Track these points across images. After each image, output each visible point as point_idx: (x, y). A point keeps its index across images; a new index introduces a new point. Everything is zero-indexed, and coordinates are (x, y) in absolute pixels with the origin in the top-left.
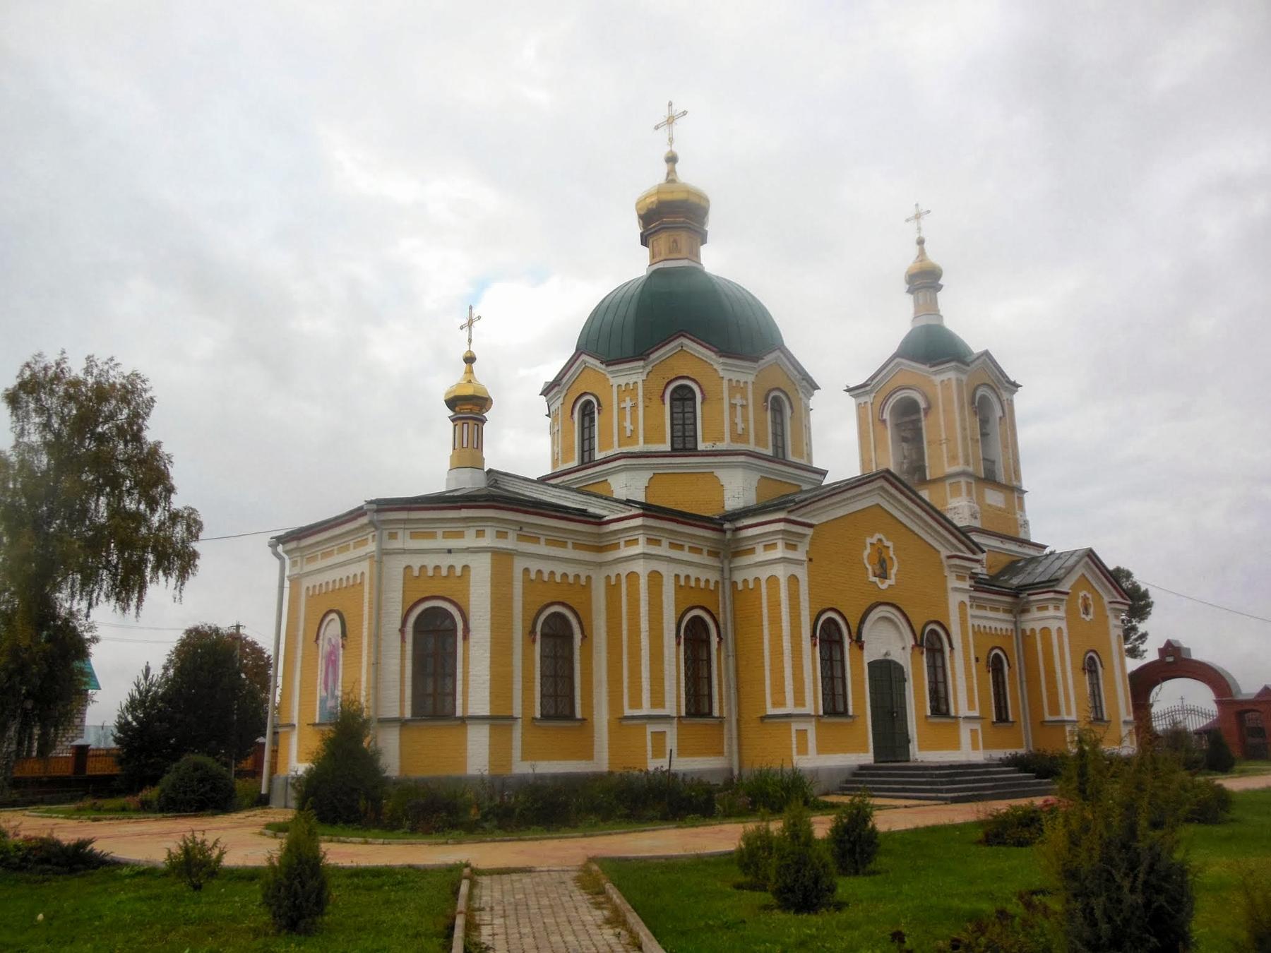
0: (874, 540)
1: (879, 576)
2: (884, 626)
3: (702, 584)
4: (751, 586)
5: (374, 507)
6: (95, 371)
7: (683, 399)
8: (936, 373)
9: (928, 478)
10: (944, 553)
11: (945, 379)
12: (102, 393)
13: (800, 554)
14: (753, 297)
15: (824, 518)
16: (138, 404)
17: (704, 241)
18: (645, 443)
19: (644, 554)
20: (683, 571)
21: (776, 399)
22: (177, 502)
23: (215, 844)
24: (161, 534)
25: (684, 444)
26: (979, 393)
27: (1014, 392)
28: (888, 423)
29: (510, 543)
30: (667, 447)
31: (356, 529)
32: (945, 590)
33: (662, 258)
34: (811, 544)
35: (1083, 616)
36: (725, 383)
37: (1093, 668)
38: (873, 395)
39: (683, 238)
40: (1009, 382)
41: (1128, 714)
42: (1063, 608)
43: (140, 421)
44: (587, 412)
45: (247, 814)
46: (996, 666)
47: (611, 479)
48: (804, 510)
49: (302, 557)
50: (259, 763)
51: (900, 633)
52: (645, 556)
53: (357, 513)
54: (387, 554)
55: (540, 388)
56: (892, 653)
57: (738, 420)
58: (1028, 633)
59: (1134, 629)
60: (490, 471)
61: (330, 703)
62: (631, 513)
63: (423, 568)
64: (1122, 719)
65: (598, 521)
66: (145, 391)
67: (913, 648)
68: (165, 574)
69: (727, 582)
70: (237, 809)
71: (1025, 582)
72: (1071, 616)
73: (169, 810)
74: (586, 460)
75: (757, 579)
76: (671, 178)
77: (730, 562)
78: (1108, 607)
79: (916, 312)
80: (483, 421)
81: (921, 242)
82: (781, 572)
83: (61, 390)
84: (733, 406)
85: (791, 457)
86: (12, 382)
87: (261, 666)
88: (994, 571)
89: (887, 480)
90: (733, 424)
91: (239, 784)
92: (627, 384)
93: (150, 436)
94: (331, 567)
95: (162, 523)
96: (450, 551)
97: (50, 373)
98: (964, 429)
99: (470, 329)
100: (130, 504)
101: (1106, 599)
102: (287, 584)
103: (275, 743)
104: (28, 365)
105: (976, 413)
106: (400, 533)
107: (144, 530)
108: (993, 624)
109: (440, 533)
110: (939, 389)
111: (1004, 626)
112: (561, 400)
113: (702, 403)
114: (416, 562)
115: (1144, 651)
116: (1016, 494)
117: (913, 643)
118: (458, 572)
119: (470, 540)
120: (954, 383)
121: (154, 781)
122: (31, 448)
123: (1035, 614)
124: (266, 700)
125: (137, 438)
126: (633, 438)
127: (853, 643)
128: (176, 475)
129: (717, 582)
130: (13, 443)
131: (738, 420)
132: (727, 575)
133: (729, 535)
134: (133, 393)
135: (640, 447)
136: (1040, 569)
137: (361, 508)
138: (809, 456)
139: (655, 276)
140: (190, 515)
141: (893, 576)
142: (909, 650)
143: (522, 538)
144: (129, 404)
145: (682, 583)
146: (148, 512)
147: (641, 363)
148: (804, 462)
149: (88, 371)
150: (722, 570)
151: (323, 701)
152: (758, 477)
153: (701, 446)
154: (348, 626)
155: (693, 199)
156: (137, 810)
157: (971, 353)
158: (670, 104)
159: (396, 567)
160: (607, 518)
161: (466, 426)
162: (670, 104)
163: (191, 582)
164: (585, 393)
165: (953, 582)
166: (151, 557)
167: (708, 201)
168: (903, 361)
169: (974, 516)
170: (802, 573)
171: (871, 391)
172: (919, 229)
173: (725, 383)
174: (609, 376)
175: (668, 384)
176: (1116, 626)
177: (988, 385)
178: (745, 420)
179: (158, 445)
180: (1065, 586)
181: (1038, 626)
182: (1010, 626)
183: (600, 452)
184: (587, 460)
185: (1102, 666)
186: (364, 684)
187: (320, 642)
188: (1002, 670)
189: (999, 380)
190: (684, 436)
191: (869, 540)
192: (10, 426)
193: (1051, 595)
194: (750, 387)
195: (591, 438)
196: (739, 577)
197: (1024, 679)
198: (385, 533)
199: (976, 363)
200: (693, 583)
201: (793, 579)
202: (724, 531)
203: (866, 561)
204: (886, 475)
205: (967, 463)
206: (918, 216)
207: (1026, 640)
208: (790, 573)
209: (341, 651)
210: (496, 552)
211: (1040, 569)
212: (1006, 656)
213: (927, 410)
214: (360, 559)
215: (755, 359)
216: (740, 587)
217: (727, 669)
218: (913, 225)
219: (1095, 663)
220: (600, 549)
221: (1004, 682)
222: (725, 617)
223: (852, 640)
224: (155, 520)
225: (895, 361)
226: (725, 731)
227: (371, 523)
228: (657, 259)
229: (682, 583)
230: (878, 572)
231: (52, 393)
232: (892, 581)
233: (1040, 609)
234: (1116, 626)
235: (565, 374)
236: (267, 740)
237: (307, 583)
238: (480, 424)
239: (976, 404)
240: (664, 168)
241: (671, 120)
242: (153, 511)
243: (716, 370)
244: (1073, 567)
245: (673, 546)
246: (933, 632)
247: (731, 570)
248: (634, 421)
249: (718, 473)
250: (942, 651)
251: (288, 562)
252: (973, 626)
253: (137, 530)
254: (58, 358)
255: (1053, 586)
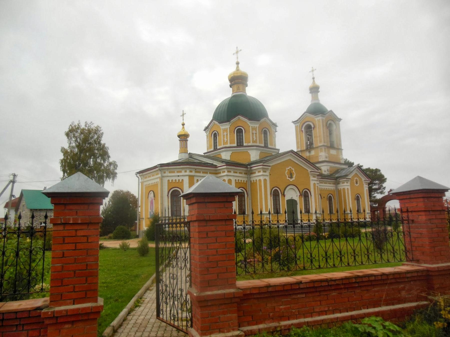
0: (289, 168)
1: (290, 178)
2: (292, 191)
3: (243, 182)
4: (255, 182)
5: (160, 166)
6: (88, 126)
7: (240, 132)
8: (316, 117)
9: (314, 147)
10: (309, 170)
11: (318, 120)
12: (90, 131)
13: (267, 173)
14: (260, 102)
15: (274, 164)
16: (99, 134)
17: (247, 86)
18: (230, 144)
19: (227, 175)
20: (237, 179)
21: (265, 131)
22: (111, 160)
23: (128, 242)
24: (107, 168)
25: (240, 144)
26: (329, 122)
27: (340, 121)
28: (304, 132)
29: (193, 173)
30: (236, 145)
31: (156, 171)
32: (310, 181)
33: (235, 92)
34: (270, 171)
35: (356, 185)
36: (251, 127)
37: (358, 199)
38: (299, 123)
39: (241, 86)
40: (339, 119)
41: (369, 211)
42: (349, 183)
43: (100, 138)
44: (215, 136)
45: (134, 239)
46: (330, 199)
47: (222, 154)
48: (267, 162)
49: (143, 177)
50: (136, 228)
51: (295, 191)
52: (227, 175)
53: (155, 167)
54: (163, 177)
55: (204, 129)
56: (293, 197)
57: (254, 137)
58: (339, 190)
59: (382, 186)
60: (190, 153)
61: (152, 213)
62: (223, 165)
63: (172, 180)
64: (367, 212)
65: (216, 166)
66: (101, 130)
67: (299, 196)
68: (109, 179)
69: (249, 181)
70: (132, 238)
71: (340, 176)
72: (352, 185)
73: (116, 239)
74: (215, 148)
75: (256, 180)
76: (238, 69)
77: (250, 176)
78: (364, 182)
79: (312, 99)
80: (187, 141)
81: (313, 78)
82: (262, 178)
83: (79, 131)
84: (253, 134)
85: (269, 146)
86: (67, 130)
87: (135, 201)
88: (331, 173)
89: (292, 152)
90: (253, 138)
91: (131, 233)
92: (225, 128)
93: (102, 142)
94: (150, 180)
95: (107, 165)
96: (178, 176)
97: (76, 127)
98: (324, 133)
99: (183, 117)
100: (99, 160)
101: (363, 179)
102: (140, 184)
103: (140, 222)
104: (71, 125)
105: (327, 128)
106: (166, 172)
107: (103, 168)
108: (329, 188)
109: (176, 171)
110: (317, 122)
111: (332, 188)
112: (208, 132)
113: (245, 133)
114: (170, 179)
115: (385, 192)
116: (340, 151)
117: (299, 194)
118: (181, 181)
119: (183, 173)
120: (321, 121)
121: (111, 232)
122: (73, 147)
123: (341, 184)
124: (137, 210)
125: (99, 143)
126: (227, 143)
127: (282, 195)
128: (110, 152)
129: (246, 181)
130: (68, 146)
131: (254, 137)
132: (249, 179)
133: (249, 169)
134: (98, 131)
135: (229, 145)
136: (344, 172)
137: (156, 166)
138: (275, 145)
139: (233, 97)
140: (114, 163)
141: (294, 178)
142: (298, 196)
143: (196, 172)
144: (97, 134)
145: (237, 181)
146: (102, 162)
147: (228, 123)
148: (273, 147)
149: (86, 126)
150: (248, 177)
151: (150, 213)
152: (259, 152)
153: (245, 144)
154: (155, 195)
155: (244, 75)
156: (108, 239)
157: (327, 110)
158: (237, 48)
159: (166, 180)
160: (218, 166)
161: (183, 142)
162: (237, 48)
163: (116, 180)
164: (214, 131)
165: (312, 178)
166: (105, 174)
167: (247, 75)
168: (308, 114)
169: (326, 158)
170: (268, 178)
171: (299, 122)
172: (313, 75)
173: (251, 127)
174: (220, 126)
175: (236, 128)
176: (366, 187)
177: (330, 120)
178: (256, 137)
179: (104, 144)
180: (350, 177)
181: (342, 188)
182: (334, 188)
183: (219, 146)
184: (215, 149)
185: (361, 198)
186: (159, 208)
187: (149, 198)
188: (332, 200)
189: (335, 118)
190: (240, 142)
191: (287, 169)
192: (67, 141)
193: (345, 179)
194: (257, 128)
195: (216, 142)
196: (252, 179)
197: (338, 202)
198: (163, 172)
199: (327, 114)
200: (240, 182)
201: (265, 180)
202: (248, 168)
203: (286, 174)
204: (292, 151)
205: (324, 142)
206: (313, 71)
207: (339, 192)
208: (264, 178)
209: (154, 200)
210: (190, 176)
211: (344, 172)
212: (333, 196)
213: (314, 128)
214: (157, 178)
215: (259, 121)
216: (252, 182)
217: (249, 202)
218: (311, 74)
219: (359, 197)
220: (216, 174)
221: (332, 203)
222: (249, 190)
223: (282, 194)
224: (105, 165)
225: (305, 114)
226: (249, 218)
227: (159, 170)
228: (234, 92)
229: (237, 181)
230: (290, 177)
231: (77, 132)
232: (294, 179)
233: (343, 183)
234: (366, 187)
235: (209, 126)
236: (137, 222)
237: (145, 183)
238: (186, 141)
239: (328, 126)
240: (236, 66)
241: (237, 52)
242: (104, 161)
243: (248, 124)
244: (353, 171)
245: (234, 172)
246: (306, 191)
247: (250, 178)
248: (227, 138)
249: (249, 151)
250: (308, 196)
251: (140, 178)
252: (319, 188)
253: (101, 167)
254: (78, 122)
255: (346, 177)
